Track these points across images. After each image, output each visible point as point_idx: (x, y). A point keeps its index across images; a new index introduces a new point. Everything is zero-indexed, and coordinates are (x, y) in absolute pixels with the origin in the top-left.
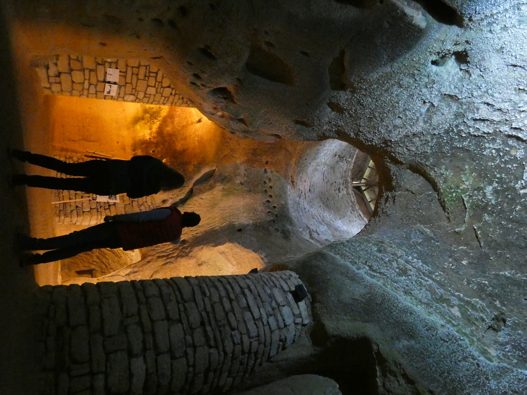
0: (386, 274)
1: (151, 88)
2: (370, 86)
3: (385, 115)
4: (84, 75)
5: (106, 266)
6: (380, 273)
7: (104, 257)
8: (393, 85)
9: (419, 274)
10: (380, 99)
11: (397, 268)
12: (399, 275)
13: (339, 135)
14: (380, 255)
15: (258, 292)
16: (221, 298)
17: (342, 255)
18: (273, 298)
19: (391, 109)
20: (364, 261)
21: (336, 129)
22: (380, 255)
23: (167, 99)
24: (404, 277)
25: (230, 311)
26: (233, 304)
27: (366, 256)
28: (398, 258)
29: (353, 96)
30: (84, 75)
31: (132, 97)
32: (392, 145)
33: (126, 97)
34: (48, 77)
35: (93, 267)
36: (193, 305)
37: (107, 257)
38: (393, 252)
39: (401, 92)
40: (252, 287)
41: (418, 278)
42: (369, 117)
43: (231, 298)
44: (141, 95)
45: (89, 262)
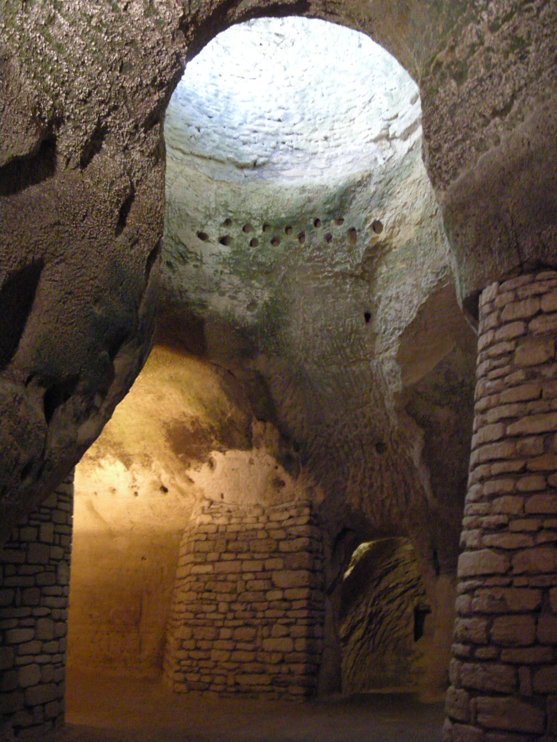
0: (517, 88)
1: (41, 534)
2: (47, 92)
3: (118, 38)
4: (24, 665)
5: (413, 587)
6: (513, 97)
7: (393, 591)
8: (48, 39)
9: (529, 10)
10: (80, 58)
11: (506, 57)
12: (522, 58)
13: (156, 123)
14: (469, 83)
15: (518, 402)
16: (516, 493)
17: (460, 164)
18: (537, 370)
19: (105, 30)
20: (481, 120)
21: (142, 130)
22: (469, 80)
23: (62, 497)
24: (531, 48)
25: (546, 480)
26: (534, 470)
27: (469, 111)
28: (482, 43)
29: (69, 117)
30: (24, 665)
31: (62, 571)
32: (193, 12)
33: (63, 581)
34: (33, 726)
35: (410, 610)
36: (520, 555)
37: (391, 586)
38: (467, 50)
39: (64, 16)
40: (505, 411)
41: (537, 15)
42: (120, 71)
43: (521, 469)
44: (57, 552)
45: (399, 618)
